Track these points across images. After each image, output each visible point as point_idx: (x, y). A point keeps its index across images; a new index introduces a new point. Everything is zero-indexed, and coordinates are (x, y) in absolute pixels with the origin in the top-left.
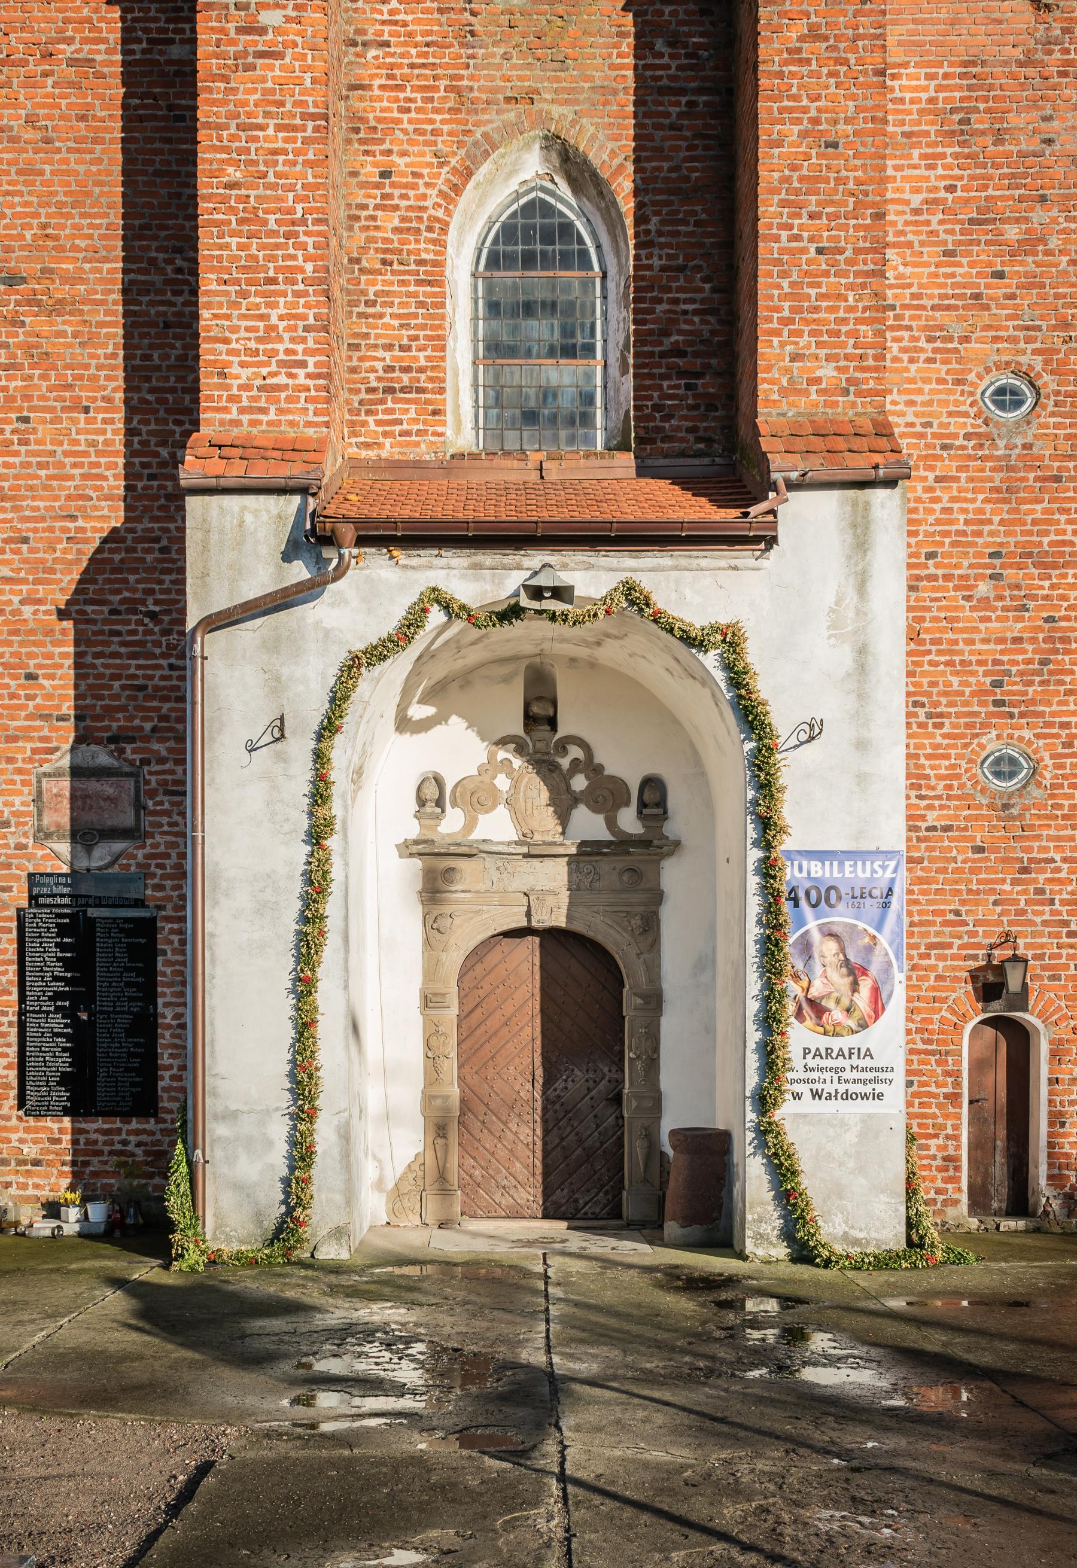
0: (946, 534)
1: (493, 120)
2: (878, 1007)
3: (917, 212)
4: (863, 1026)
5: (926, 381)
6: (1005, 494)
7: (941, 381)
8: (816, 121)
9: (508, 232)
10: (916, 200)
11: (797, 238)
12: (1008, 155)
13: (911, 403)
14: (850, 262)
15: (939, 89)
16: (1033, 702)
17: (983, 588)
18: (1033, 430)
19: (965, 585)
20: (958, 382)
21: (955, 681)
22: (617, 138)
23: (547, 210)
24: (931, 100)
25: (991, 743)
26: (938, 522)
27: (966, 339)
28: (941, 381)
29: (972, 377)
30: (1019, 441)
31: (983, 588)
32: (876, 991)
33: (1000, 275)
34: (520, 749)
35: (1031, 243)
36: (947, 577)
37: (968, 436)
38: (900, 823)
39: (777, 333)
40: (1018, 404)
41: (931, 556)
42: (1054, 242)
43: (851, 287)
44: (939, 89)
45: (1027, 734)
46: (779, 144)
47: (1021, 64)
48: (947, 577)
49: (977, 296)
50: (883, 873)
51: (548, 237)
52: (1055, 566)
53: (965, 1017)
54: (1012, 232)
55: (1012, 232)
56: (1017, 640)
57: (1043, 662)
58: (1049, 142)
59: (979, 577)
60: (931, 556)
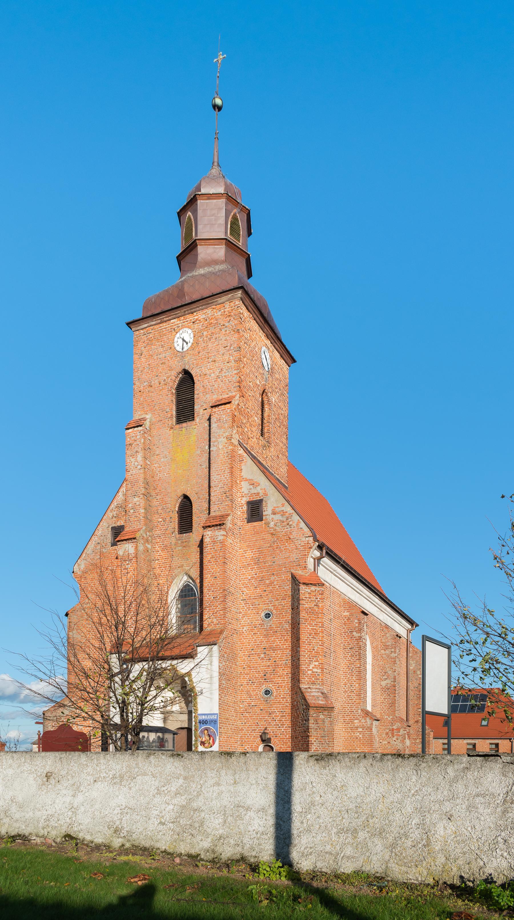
0: (255, 645)
1: (176, 571)
2: (214, 743)
3: (250, 580)
4: (211, 747)
5: (251, 614)
6: (266, 636)
7: (254, 614)
8: (213, 573)
9: (182, 591)
10: (249, 577)
11: (210, 596)
12: (267, 566)
13: (249, 619)
14: (219, 599)
15: (254, 554)
16: (272, 679)
17: (262, 656)
18: (272, 622)
19: (259, 655)
20: (258, 614)
21: (257, 675)
22: (197, 572)
23: (188, 585)
24: (252, 557)
25: (264, 688)
26: (254, 642)
27: (259, 605)
28: (254, 614)
29: (260, 612)
30: (269, 625)
31: (262, 656)
32: (213, 740)
33: (265, 591)
34: (180, 693)
35: (271, 583)
36: (255, 654)
37: (259, 625)
38: (217, 707)
39: (206, 614)
40: (269, 617)
41: (252, 650)
42: (275, 583)
43: (219, 604)
44: (254, 554)
45: (271, 685)
46: (207, 578)
47: (269, 547)
48: (255, 654)
49: (261, 596)
50: (215, 717)
51: (189, 591)
52: (276, 650)
53: (259, 745)
54: (267, 582)
55: (267, 582)
56: (269, 666)
57: (274, 670)
58: (274, 562)
59: (262, 653)
60: (252, 650)
